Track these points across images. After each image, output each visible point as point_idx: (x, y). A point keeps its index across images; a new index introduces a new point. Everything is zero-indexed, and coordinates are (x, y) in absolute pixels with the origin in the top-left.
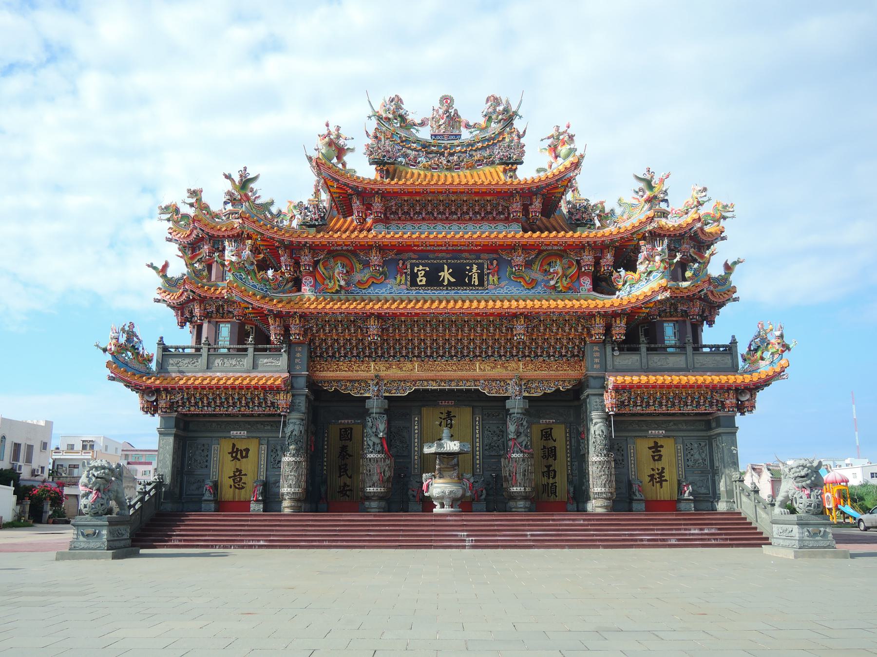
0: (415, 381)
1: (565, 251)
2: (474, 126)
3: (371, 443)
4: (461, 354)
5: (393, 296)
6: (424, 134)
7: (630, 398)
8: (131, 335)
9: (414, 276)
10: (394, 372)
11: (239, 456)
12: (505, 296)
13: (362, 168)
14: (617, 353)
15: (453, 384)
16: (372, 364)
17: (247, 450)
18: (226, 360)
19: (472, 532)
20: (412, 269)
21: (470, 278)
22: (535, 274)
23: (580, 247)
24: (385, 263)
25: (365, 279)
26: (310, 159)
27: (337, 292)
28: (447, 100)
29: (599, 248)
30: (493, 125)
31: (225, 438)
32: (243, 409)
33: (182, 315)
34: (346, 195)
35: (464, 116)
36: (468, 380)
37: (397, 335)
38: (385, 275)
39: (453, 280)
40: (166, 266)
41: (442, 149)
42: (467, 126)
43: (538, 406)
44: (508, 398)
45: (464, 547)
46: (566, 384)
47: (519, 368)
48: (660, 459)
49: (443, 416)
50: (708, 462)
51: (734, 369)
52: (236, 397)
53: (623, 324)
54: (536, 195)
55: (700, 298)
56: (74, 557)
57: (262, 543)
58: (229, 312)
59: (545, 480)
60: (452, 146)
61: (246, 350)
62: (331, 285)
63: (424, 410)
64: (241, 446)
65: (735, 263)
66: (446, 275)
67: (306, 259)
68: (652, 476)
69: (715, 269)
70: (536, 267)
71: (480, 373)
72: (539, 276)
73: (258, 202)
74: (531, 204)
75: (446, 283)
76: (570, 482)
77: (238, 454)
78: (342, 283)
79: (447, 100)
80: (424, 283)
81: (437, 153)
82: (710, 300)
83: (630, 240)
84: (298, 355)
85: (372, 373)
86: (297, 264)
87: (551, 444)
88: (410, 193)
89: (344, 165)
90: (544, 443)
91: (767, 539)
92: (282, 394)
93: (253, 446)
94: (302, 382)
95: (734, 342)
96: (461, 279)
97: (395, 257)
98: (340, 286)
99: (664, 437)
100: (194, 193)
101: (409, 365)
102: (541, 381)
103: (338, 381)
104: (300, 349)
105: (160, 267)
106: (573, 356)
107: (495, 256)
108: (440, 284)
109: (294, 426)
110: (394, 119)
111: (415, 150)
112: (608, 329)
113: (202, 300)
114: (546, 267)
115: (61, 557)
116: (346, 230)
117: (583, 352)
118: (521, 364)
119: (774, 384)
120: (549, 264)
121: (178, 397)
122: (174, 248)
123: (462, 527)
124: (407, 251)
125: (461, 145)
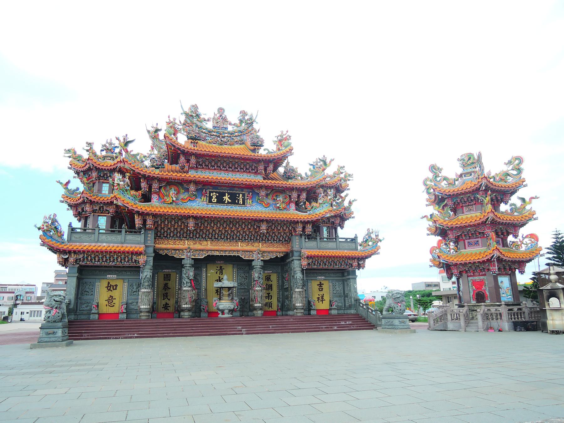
0: (208, 251)
1: (284, 191)
2: (234, 125)
3: (185, 282)
4: (232, 238)
5: (200, 206)
6: (209, 125)
7: (312, 262)
8: (54, 221)
9: (211, 198)
10: (198, 246)
11: (112, 289)
12: (253, 209)
13: (182, 139)
14: (307, 240)
15: (227, 253)
16: (186, 241)
17: (116, 286)
18: (108, 237)
19: (244, 326)
20: (210, 194)
21: (239, 200)
22: (267, 201)
23: (292, 189)
24: (197, 190)
25: (185, 198)
26: (149, 132)
27: (171, 203)
28: (221, 110)
29: (300, 190)
30: (243, 124)
31: (104, 279)
32: (118, 263)
33: (76, 211)
34: (175, 154)
35: (229, 119)
36: (234, 251)
37: (204, 226)
38: (196, 196)
39: (230, 201)
40: (68, 182)
41: (219, 133)
42: (230, 124)
43: (268, 264)
44: (253, 260)
45: (242, 334)
46: (281, 254)
47: (259, 246)
48: (322, 290)
49: (218, 269)
50: (342, 292)
51: (356, 249)
52: (115, 257)
53: (310, 227)
54: (271, 162)
55: (340, 216)
56: (42, 347)
57: (136, 335)
58: (107, 210)
59: (267, 301)
60: (224, 133)
61: (121, 232)
62: (168, 200)
63: (209, 266)
64: (113, 283)
65: (353, 201)
66: (226, 198)
67: (155, 185)
68: (318, 298)
69: (346, 204)
70: (270, 197)
71: (240, 248)
72: (271, 202)
73: (132, 153)
74: (268, 167)
75: (226, 202)
76: (278, 301)
77: (110, 287)
78: (174, 199)
79: (221, 110)
80: (215, 201)
81: (216, 136)
82: (341, 218)
83: (315, 187)
84: (149, 235)
85: (186, 246)
86: (150, 187)
87: (270, 283)
88: (211, 156)
89: (177, 138)
90: (266, 282)
91: (374, 326)
92: (142, 256)
93: (119, 283)
94: (151, 250)
95: (356, 237)
96: (234, 201)
97: (203, 186)
98: (173, 200)
99: (324, 280)
100: (89, 144)
101: (205, 243)
102: (269, 252)
103: (167, 249)
104: (150, 232)
105: (64, 182)
106: (285, 241)
107: (250, 190)
108: (224, 202)
109: (147, 273)
110: (193, 116)
111: (204, 133)
112: (304, 228)
113: (91, 203)
114: (275, 198)
115: (32, 347)
116: (171, 171)
117: (290, 239)
118: (260, 244)
119: (372, 256)
120: (276, 196)
121: (81, 256)
122: (72, 173)
123: (238, 324)
124: (207, 185)
125: (229, 133)
